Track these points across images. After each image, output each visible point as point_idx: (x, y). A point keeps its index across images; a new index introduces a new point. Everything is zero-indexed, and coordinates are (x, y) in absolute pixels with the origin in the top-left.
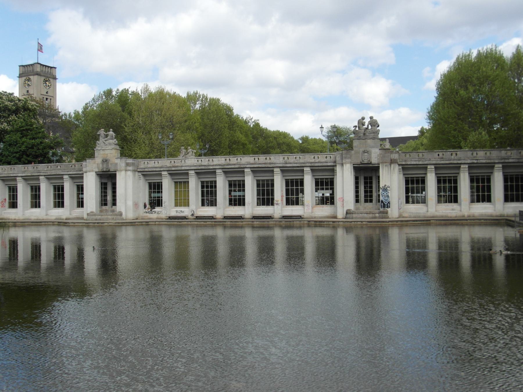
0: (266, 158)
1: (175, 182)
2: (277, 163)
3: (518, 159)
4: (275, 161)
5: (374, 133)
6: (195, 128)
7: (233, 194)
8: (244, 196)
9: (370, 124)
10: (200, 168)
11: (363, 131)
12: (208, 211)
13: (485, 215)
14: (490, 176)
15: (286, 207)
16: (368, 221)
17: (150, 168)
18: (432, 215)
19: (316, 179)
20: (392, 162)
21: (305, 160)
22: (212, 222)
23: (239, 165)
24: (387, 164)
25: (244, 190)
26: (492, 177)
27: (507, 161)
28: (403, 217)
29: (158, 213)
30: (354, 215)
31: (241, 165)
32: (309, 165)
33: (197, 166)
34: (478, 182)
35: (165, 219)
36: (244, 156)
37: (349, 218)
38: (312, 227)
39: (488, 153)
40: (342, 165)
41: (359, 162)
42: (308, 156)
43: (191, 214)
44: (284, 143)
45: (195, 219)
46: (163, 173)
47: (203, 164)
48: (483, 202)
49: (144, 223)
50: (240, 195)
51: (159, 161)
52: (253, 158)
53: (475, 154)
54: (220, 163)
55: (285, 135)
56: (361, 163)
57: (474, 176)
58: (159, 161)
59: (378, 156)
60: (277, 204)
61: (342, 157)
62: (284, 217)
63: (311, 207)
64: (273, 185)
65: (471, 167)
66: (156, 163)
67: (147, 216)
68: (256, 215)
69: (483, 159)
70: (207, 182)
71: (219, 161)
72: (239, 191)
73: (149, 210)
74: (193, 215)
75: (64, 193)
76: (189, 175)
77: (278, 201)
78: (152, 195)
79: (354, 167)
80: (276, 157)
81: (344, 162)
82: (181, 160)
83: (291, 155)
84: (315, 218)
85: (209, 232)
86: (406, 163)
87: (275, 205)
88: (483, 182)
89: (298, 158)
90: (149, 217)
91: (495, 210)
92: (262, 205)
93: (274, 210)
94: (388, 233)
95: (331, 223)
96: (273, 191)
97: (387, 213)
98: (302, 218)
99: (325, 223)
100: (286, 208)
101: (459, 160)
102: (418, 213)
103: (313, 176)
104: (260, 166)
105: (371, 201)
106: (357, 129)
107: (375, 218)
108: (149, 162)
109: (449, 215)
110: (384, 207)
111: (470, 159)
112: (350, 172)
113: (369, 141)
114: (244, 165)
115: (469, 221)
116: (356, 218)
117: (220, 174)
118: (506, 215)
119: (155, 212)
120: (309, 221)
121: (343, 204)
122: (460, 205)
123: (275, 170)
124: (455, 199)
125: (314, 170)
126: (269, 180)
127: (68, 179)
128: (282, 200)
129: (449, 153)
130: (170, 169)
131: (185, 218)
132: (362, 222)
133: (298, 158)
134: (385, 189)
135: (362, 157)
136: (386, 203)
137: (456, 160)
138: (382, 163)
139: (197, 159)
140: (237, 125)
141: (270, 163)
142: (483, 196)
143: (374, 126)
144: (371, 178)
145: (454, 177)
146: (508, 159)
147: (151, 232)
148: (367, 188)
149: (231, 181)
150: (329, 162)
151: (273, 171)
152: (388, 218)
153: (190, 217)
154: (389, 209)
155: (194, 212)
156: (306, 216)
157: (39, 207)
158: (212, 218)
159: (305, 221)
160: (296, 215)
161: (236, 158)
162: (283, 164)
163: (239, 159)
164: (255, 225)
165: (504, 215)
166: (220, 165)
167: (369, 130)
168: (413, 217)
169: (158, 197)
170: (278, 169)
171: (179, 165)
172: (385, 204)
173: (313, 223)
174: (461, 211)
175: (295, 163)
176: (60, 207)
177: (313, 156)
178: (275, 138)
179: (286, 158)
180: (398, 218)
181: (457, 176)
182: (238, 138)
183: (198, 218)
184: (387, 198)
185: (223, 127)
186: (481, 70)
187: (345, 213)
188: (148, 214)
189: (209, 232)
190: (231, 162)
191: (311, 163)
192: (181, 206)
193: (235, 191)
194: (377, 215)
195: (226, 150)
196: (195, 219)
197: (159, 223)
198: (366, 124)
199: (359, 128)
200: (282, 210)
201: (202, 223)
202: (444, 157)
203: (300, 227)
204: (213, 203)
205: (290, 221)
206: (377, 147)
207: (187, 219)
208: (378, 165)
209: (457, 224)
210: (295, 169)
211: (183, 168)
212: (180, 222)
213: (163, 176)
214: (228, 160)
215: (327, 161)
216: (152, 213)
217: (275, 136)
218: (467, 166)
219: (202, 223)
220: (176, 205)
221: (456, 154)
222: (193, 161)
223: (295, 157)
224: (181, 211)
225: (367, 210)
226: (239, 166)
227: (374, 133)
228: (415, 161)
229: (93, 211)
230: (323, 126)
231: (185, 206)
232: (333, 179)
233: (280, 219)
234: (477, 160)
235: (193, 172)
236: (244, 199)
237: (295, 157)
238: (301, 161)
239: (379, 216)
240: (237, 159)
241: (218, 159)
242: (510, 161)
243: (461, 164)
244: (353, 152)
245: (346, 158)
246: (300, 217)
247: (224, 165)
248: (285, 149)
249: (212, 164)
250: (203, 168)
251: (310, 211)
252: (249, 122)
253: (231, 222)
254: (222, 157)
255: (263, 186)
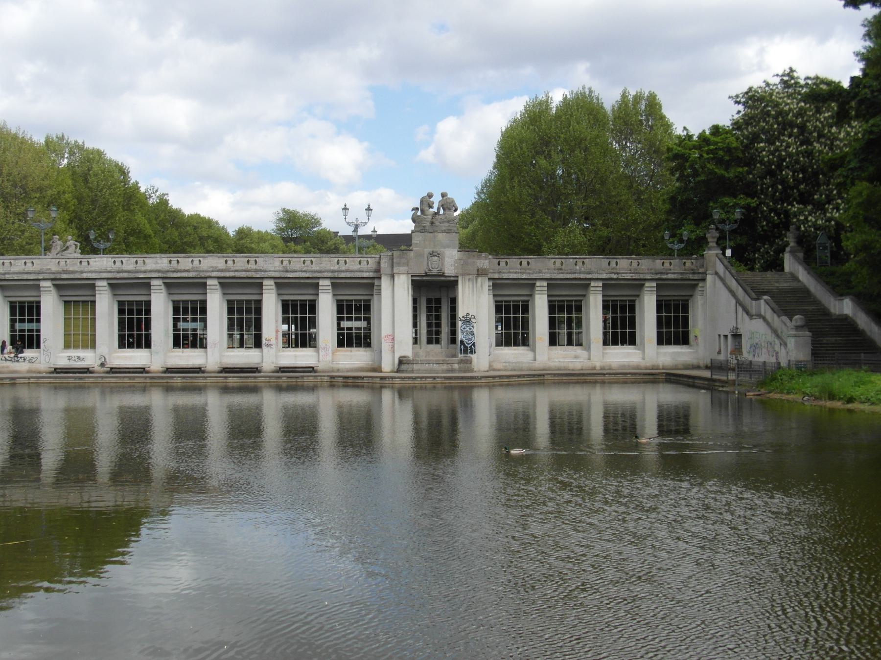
0: (248, 261)
1: (67, 303)
2: (270, 271)
3: (682, 274)
4: (265, 267)
5: (449, 221)
6: (64, 201)
7: (18, 326)
8: (38, 331)
9: (442, 206)
10: (118, 276)
11: (430, 217)
12: (135, 357)
13: (629, 367)
14: (687, 301)
15: (283, 351)
16: (445, 377)
17: (17, 273)
18: (542, 366)
19: (338, 301)
20: (480, 273)
21: (322, 265)
22: (146, 378)
23: (197, 271)
24: (471, 276)
25: (38, 321)
26: (583, 303)
27: (664, 277)
28: (494, 370)
29: (31, 361)
30: (416, 367)
31: (200, 271)
32: (330, 275)
33: (114, 272)
34: (614, 311)
35: (46, 373)
36: (206, 255)
37: (406, 372)
38: (339, 387)
39: (635, 263)
40: (392, 276)
41: (422, 273)
42: (327, 259)
43: (99, 362)
44: (209, 237)
45: (107, 372)
46: (43, 284)
47: (126, 267)
48: (622, 344)
49: (7, 381)
50: (360, 326)
51: (34, 261)
52: (223, 260)
53: (613, 264)
54: (158, 267)
55: (209, 223)
56: (426, 273)
57: (617, 301)
58: (34, 261)
59: (456, 261)
60: (268, 346)
61: (393, 262)
62: (282, 370)
63: (330, 351)
64: (148, 311)
65: (607, 285)
66: (29, 264)
67: (8, 367)
68: (229, 366)
69: (626, 273)
70: (130, 303)
71: (156, 263)
72: (30, 321)
73: (12, 355)
74: (102, 365)
75: (657, 313)
76: (97, 288)
77: (269, 340)
78: (18, 326)
79: (412, 281)
80: (267, 259)
81: (395, 271)
82: (79, 260)
83: (295, 255)
84: (338, 370)
85: (136, 400)
86: (501, 277)
87: (264, 347)
88: (623, 311)
89: (308, 263)
90: (11, 369)
91: (643, 359)
92: (192, 347)
93: (263, 356)
94: (471, 398)
95: (378, 381)
96: (148, 322)
97: (469, 362)
98: (316, 372)
99: (365, 380)
100: (282, 353)
101: (590, 273)
102: (519, 362)
103: (224, 294)
104: (237, 274)
105: (438, 341)
106: (419, 213)
107: (452, 371)
108: (12, 261)
109: (571, 366)
110: (465, 352)
111: (607, 271)
112: (406, 289)
113: (440, 236)
114: (207, 271)
115: (607, 377)
116: (418, 371)
117: (158, 287)
118: (661, 367)
119: (25, 360)
120: (332, 377)
121: (393, 347)
122: (534, 350)
123: (265, 282)
124: (144, 342)
125: (281, 284)
126: (251, 301)
127: (271, 287)
128: (277, 339)
129: (571, 260)
130: (58, 276)
131: (87, 370)
132: (434, 378)
133: (308, 263)
134: (468, 321)
135: (428, 263)
136: (469, 346)
137: (584, 273)
138: (462, 274)
139: (113, 260)
140: (137, 200)
141: (256, 271)
142: (623, 334)
143: (450, 209)
144: (438, 301)
145: (576, 301)
146: (667, 274)
147: (16, 400)
148: (431, 318)
149: (179, 301)
150: (366, 272)
151: (260, 285)
152: (472, 371)
153: (97, 368)
154: (473, 356)
155: (105, 360)
156: (321, 366)
157: (38, 346)
158: (143, 370)
159: (324, 376)
160: (304, 366)
161: (190, 259)
162: (280, 271)
163: (196, 261)
164: (230, 385)
165: (659, 366)
166: (159, 271)
167: (440, 217)
168: (511, 370)
169: (29, 331)
170: (272, 282)
171: (76, 268)
172: (467, 347)
173: (340, 380)
174: (589, 359)
175: (305, 271)
176: (617, 344)
177: (336, 260)
178: (195, 228)
179: (286, 263)
180: (487, 371)
181: (581, 301)
182: (138, 225)
183: (113, 370)
184: (470, 337)
185: (116, 204)
186: (571, 127)
187: (397, 362)
188: (9, 363)
189: (136, 400)
190: (182, 266)
191: (333, 271)
192: (76, 347)
193: (185, 320)
194: (456, 366)
195: (119, 245)
196: (107, 372)
197: (35, 381)
198: (436, 206)
199: (423, 211)
200: (276, 356)
201: (126, 380)
202: (563, 267)
203: (313, 388)
204: (144, 342)
205: (297, 377)
206: (454, 248)
207: (91, 372)
208: (456, 279)
209: (585, 382)
210: (302, 281)
211: (85, 275)
212: (81, 378)
213: (42, 289)
214: (174, 262)
215: (361, 269)
216: (18, 361)
217: (195, 225)
218: (600, 284)
219: (126, 380)
220: (67, 346)
221: (583, 263)
222: (105, 262)
223: (303, 259)
224: (79, 357)
225: (431, 358)
226: (196, 273)
227: (449, 221)
228: (516, 273)
229: (403, 355)
230: (371, 207)
231: (85, 347)
232: (315, 301)
233: (274, 372)
234: (618, 273)
235: (327, 282)
236: (38, 337)
237: (303, 259)
238: (315, 267)
239: (460, 367)
240: (192, 261)
241: (154, 260)
242: (670, 276)
243: (591, 279)
244: (412, 254)
245: (399, 264)
246: (312, 369)
247: (168, 271)
248: (211, 248)
249: (143, 269)
250: (125, 275)
251: (329, 358)
252: (151, 197)
253: (184, 378)
254: (163, 255)
255: (240, 311)
